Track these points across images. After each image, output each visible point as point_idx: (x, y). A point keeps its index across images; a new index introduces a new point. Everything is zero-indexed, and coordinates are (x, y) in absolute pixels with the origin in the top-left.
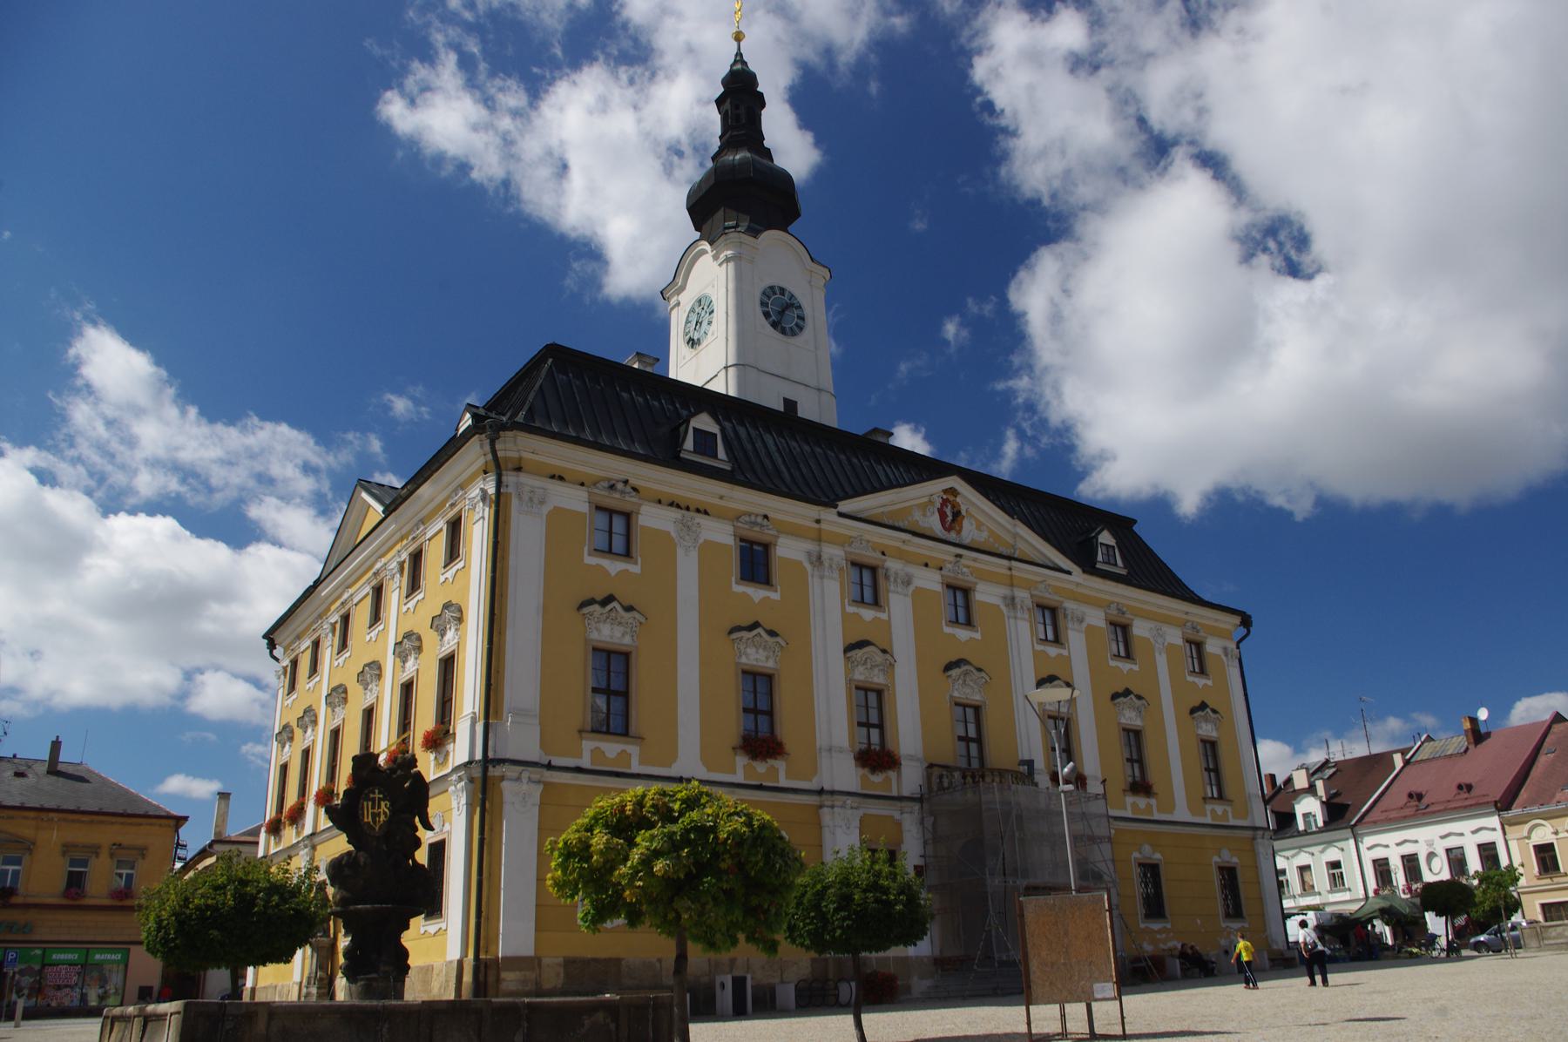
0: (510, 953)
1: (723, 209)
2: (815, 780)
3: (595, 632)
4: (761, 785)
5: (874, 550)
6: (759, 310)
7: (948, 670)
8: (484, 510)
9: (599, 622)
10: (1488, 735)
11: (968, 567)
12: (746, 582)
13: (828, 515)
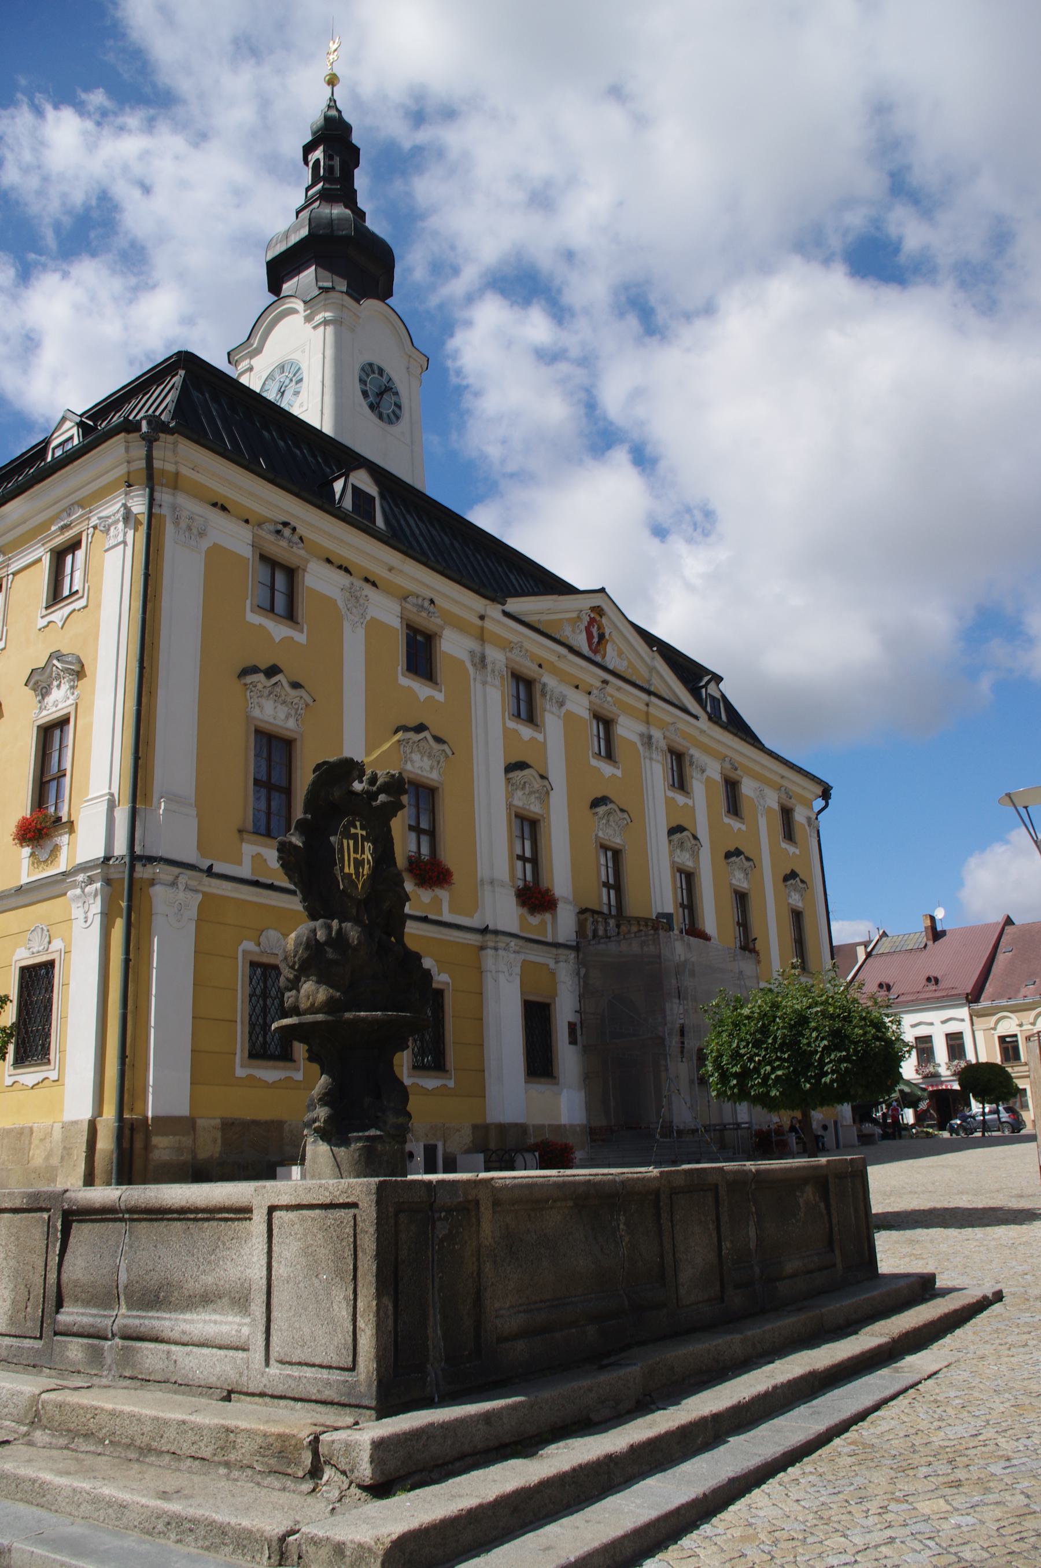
0: (162, 1112)
1: (314, 267)
2: (476, 916)
3: (257, 708)
4: (426, 917)
5: (532, 661)
6: (358, 387)
7: (595, 807)
8: (125, 534)
9: (261, 696)
10: (943, 933)
11: (612, 696)
12: (412, 675)
13: (494, 611)
